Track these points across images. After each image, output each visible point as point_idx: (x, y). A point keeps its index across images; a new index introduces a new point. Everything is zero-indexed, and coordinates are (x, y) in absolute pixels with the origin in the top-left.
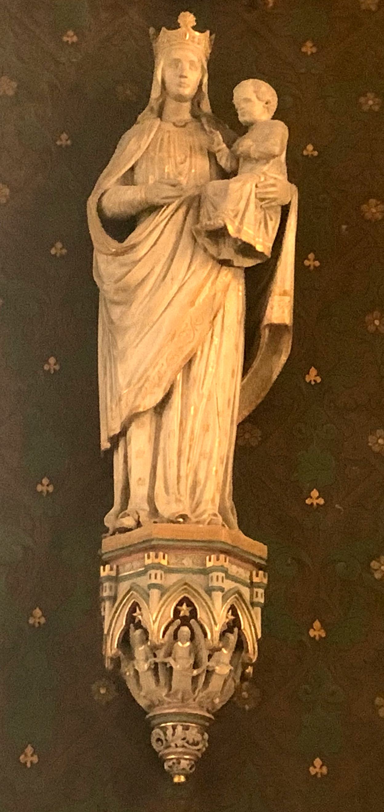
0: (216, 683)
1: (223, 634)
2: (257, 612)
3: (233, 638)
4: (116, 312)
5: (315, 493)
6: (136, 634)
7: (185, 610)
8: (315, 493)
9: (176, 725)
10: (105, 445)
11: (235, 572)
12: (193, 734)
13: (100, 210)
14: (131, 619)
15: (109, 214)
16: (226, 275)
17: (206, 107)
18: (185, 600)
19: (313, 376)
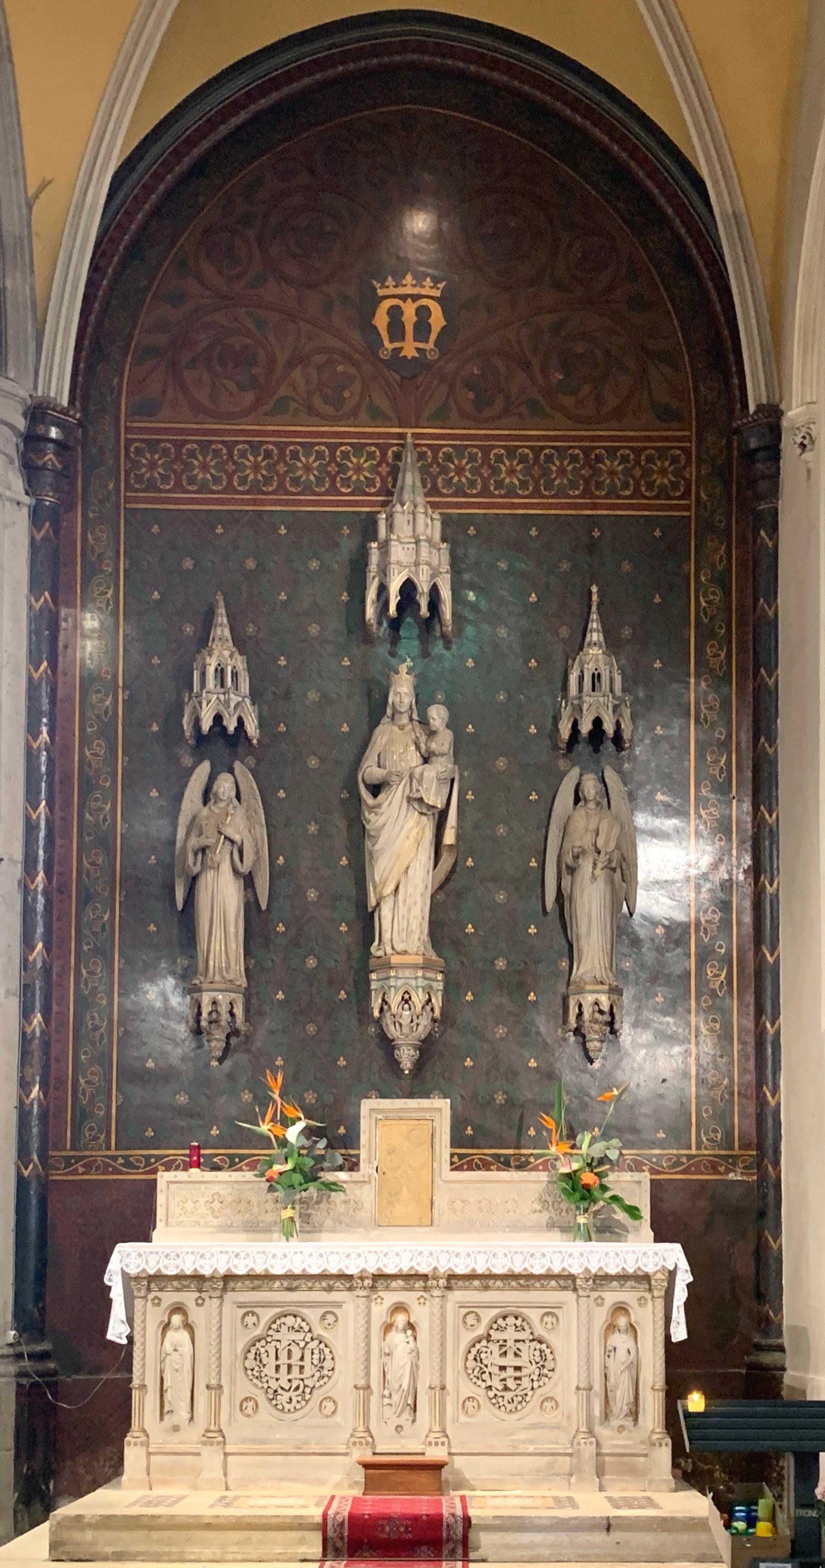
0: (420, 1028)
1: (423, 1008)
2: (440, 993)
3: (428, 1008)
4: (371, 817)
5: (470, 926)
6: (386, 1007)
7: (406, 996)
8: (470, 926)
9: (367, 786)
10: (370, 910)
11: (399, 690)
12: (412, 1052)
13: (363, 780)
14: (383, 1000)
15: (368, 782)
16: (424, 818)
17: (415, 717)
18: (407, 992)
19: (470, 862)
